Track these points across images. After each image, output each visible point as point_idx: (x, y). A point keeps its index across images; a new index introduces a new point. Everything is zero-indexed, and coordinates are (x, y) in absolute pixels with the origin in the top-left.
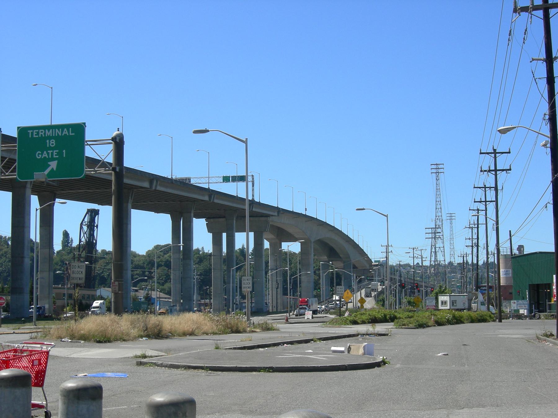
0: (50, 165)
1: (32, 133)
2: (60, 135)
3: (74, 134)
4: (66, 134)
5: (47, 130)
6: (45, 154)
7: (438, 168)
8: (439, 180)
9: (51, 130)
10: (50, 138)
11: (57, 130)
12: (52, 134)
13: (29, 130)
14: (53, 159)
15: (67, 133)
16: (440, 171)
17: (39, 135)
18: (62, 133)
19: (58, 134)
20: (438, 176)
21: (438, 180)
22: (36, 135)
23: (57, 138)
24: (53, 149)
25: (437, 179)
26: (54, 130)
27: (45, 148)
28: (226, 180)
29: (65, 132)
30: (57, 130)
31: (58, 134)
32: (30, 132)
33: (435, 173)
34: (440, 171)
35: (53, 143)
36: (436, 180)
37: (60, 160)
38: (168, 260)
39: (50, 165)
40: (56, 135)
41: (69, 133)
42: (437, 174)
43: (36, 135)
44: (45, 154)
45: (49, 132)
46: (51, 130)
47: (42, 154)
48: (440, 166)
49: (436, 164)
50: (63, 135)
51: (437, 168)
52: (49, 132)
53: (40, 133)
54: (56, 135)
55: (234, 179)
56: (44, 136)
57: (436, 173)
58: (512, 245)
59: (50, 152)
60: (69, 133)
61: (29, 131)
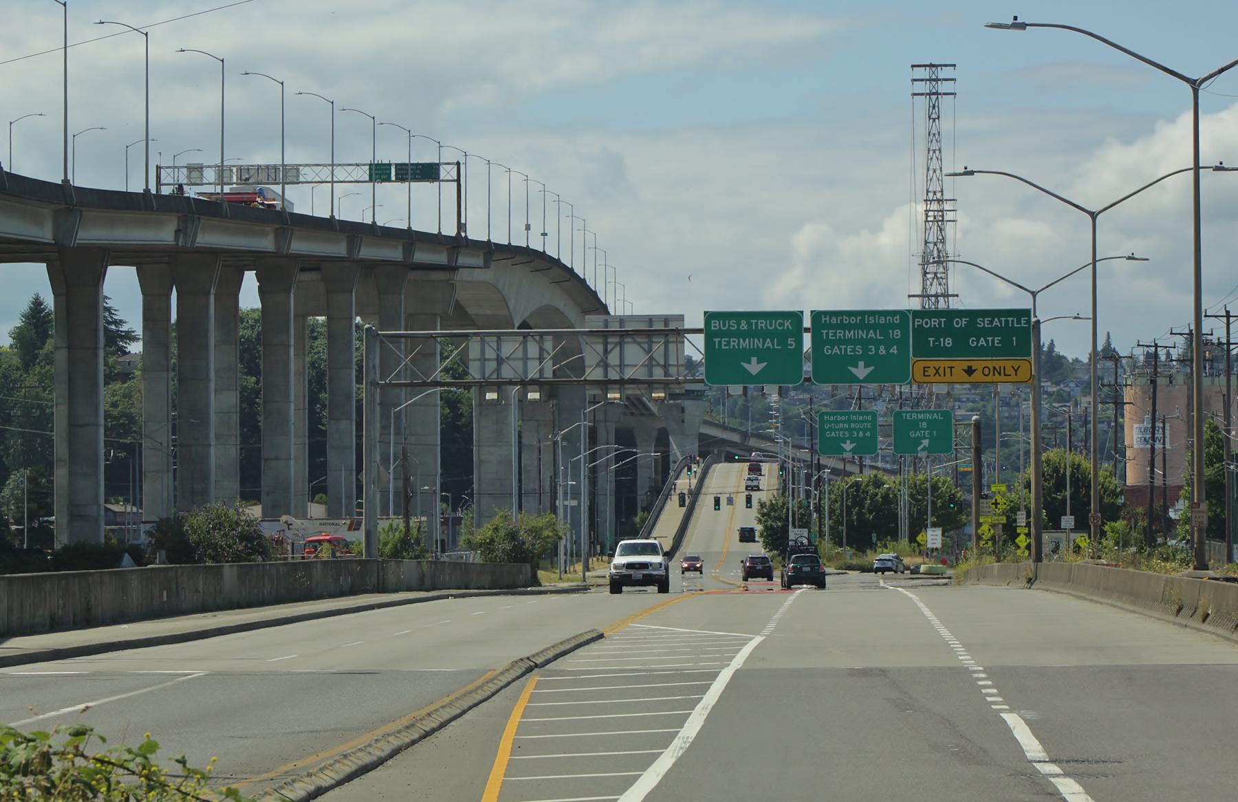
0: (922, 443)
1: (906, 416)
2: (761, 347)
3: (780, 347)
4: (769, 347)
5: (741, 340)
6: (918, 434)
7: (937, 80)
8: (938, 118)
9: (747, 340)
10: (922, 421)
11: (756, 340)
12: (750, 347)
13: (715, 338)
14: (925, 438)
15: (770, 345)
16: (943, 87)
17: (730, 347)
18: (763, 346)
19: (757, 345)
20: (934, 107)
21: (934, 120)
22: (725, 345)
23: (928, 421)
24: (925, 430)
25: (934, 116)
26: (752, 340)
27: (917, 429)
28: (381, 175)
29: (768, 343)
30: (756, 340)
31: (757, 345)
32: (904, 414)
33: (927, 94)
34: (943, 87)
35: (924, 425)
36: (930, 118)
37: (932, 439)
38: (49, 734)
39: (922, 443)
40: (755, 347)
41: (773, 345)
42: (934, 97)
43: (725, 345)
44: (918, 434)
45: (744, 342)
46: (747, 340)
47: (915, 434)
48: (943, 73)
49: (931, 66)
50: (765, 347)
51: (934, 80)
52: (744, 342)
53: (913, 416)
54: (755, 347)
55: (402, 174)
56: (737, 347)
57: (930, 94)
58: (1231, 333)
59: (922, 432)
60: (773, 345)
61: (715, 339)
